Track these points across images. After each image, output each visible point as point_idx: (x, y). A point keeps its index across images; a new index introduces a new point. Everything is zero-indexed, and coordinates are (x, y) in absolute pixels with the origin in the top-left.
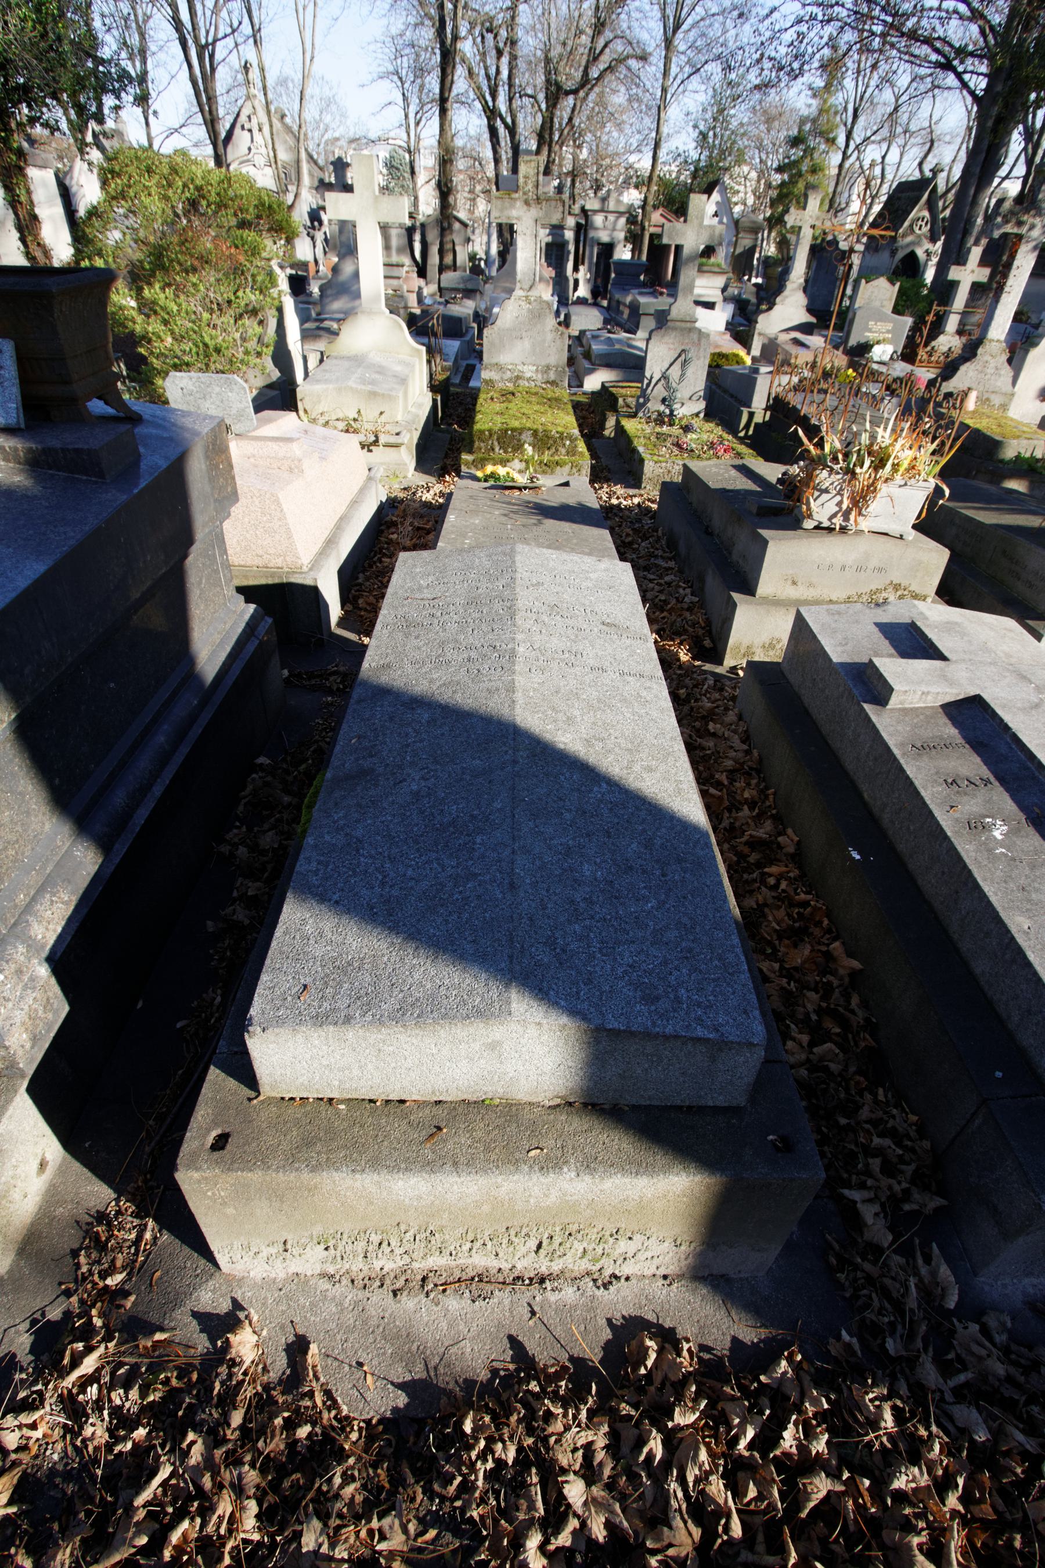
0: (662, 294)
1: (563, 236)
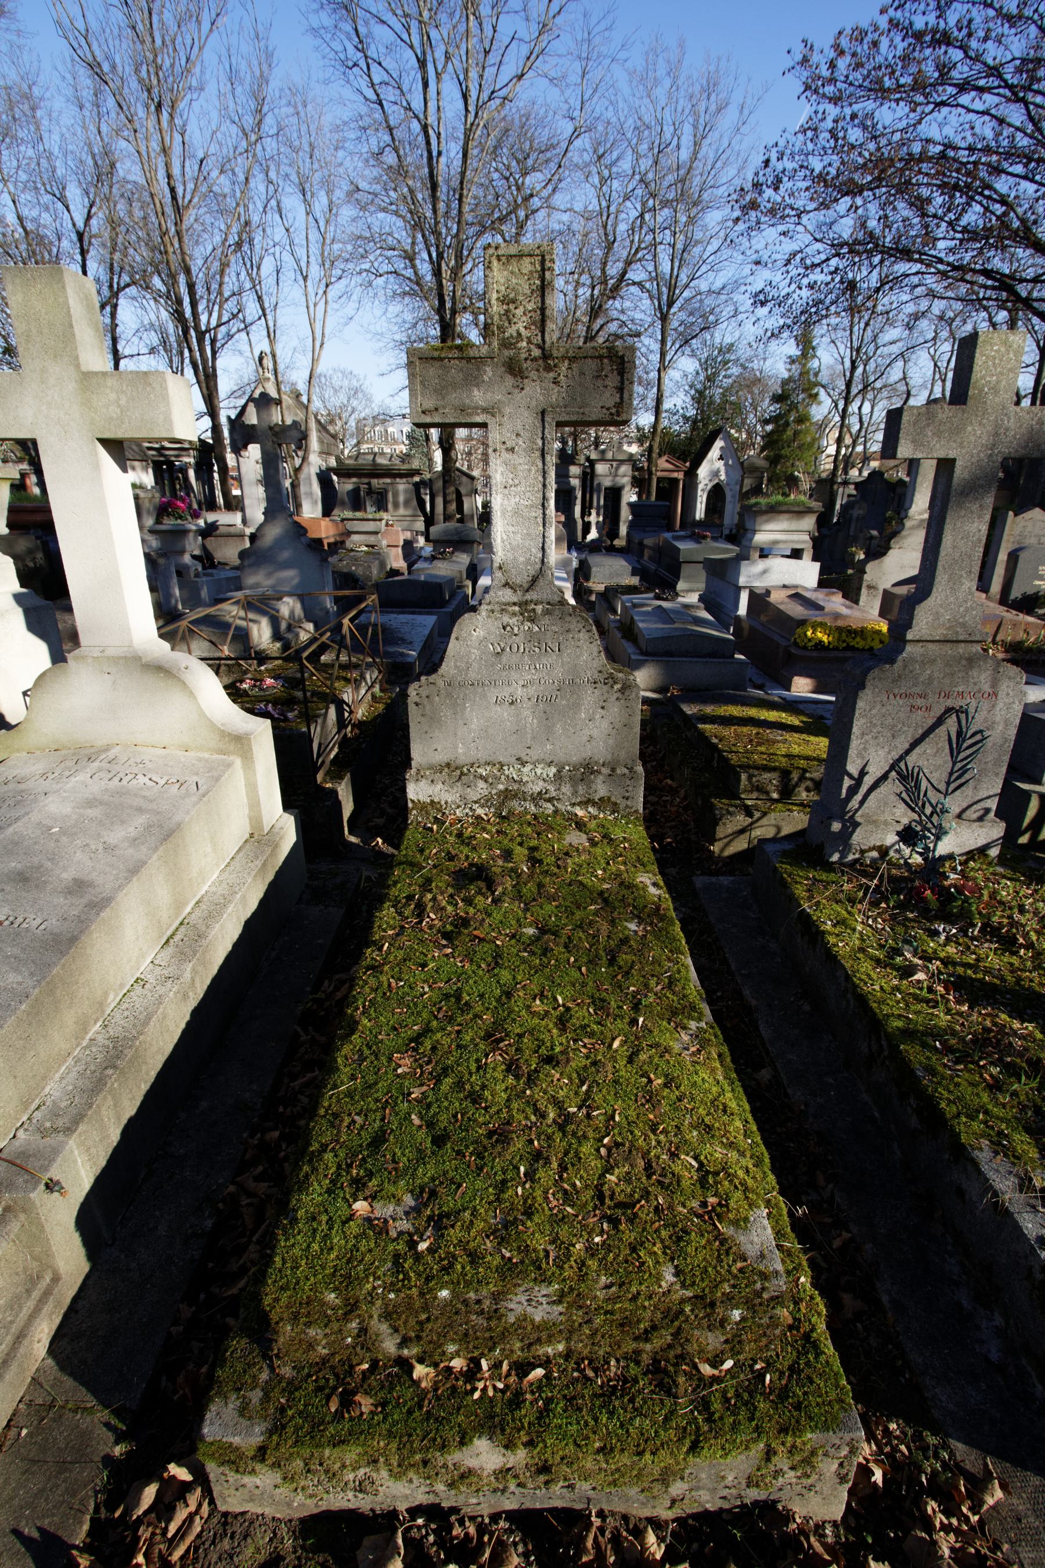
0: (705, 537)
1: (569, 483)
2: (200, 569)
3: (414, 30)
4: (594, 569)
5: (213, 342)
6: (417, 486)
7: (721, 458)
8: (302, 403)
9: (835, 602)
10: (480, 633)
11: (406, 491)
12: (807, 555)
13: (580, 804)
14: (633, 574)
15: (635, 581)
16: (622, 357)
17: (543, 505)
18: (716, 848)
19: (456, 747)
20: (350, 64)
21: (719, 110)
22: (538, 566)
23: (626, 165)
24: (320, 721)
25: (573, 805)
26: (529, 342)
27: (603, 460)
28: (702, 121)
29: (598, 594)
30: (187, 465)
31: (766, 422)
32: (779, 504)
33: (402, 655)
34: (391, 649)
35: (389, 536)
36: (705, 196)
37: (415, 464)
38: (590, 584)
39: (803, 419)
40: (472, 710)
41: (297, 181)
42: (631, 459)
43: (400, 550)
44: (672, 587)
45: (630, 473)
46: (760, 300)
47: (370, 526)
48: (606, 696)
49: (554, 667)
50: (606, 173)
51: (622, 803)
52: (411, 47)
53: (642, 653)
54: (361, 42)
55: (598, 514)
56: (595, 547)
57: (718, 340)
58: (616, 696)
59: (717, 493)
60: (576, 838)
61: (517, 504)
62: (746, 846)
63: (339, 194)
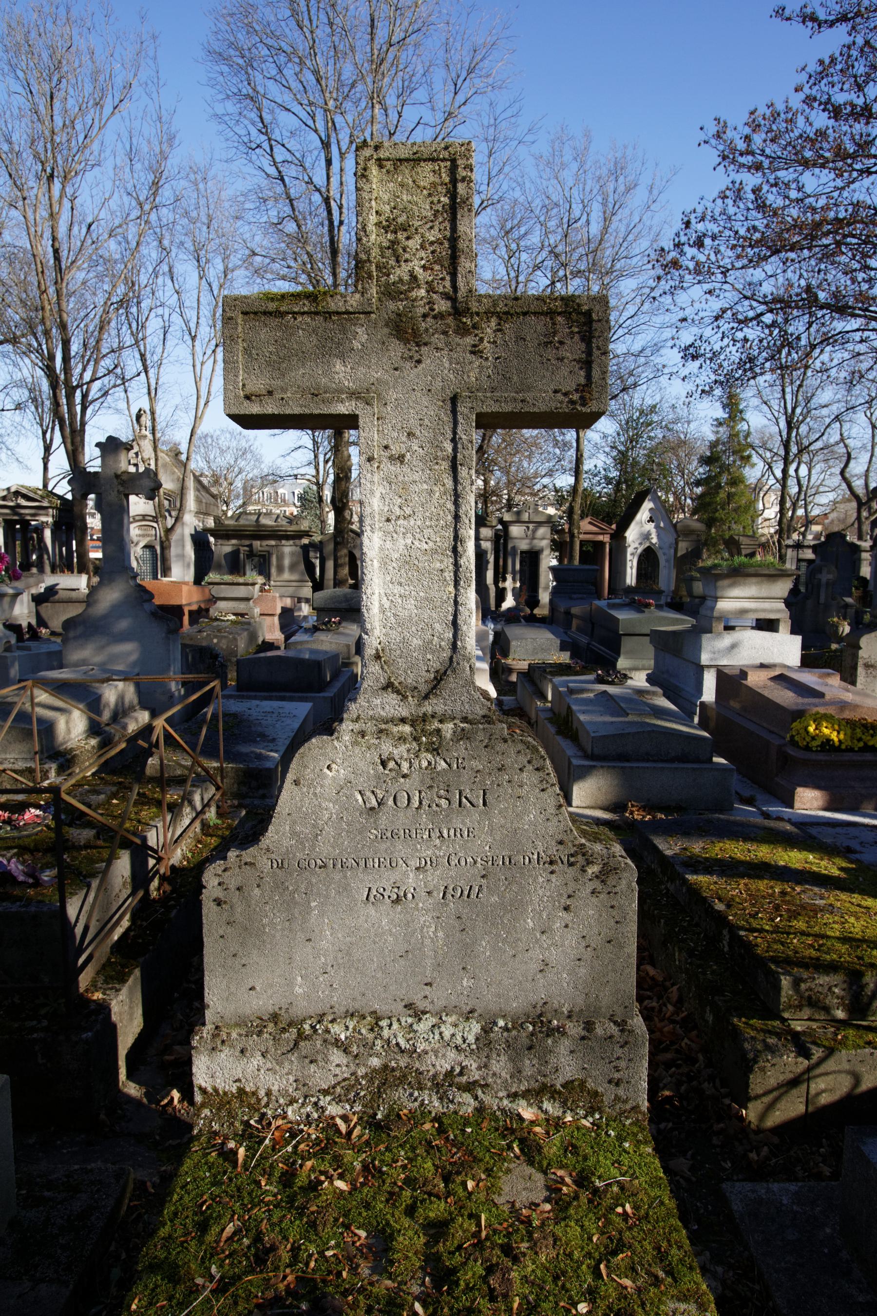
0: (648, 606)
2: (13, 641)
3: (319, 117)
4: (513, 644)
5: (85, 396)
6: (305, 549)
7: (651, 520)
8: (181, 462)
9: (831, 684)
10: (340, 772)
11: (292, 554)
12: (785, 627)
13: (526, 1094)
14: (563, 648)
15: (565, 658)
16: (589, 313)
17: (455, 550)
18: (751, 1113)
19: (291, 984)
20: (254, 146)
21: (628, 190)
22: (446, 654)
23: (535, 239)
24: (95, 883)
25: (513, 1096)
26: (431, 289)
27: (518, 521)
28: (611, 200)
29: (521, 674)
30: (43, 525)
31: (698, 483)
32: (742, 565)
33: (260, 757)
34: (245, 749)
35: (265, 606)
36: (618, 266)
37: (304, 525)
38: (509, 661)
39: (737, 481)
40: (322, 914)
41: (192, 248)
42: (549, 521)
43: (276, 619)
44: (609, 664)
45: (549, 536)
46: (691, 353)
47: (241, 591)
48: (572, 886)
49: (479, 836)
50: (514, 246)
51: (608, 1093)
52: (316, 131)
53: (586, 757)
54: (265, 126)
55: (514, 579)
56: (512, 617)
57: (637, 402)
58: (590, 886)
59: (648, 557)
60: (521, 1187)
61: (408, 548)
62: (802, 1108)
63: (234, 260)
